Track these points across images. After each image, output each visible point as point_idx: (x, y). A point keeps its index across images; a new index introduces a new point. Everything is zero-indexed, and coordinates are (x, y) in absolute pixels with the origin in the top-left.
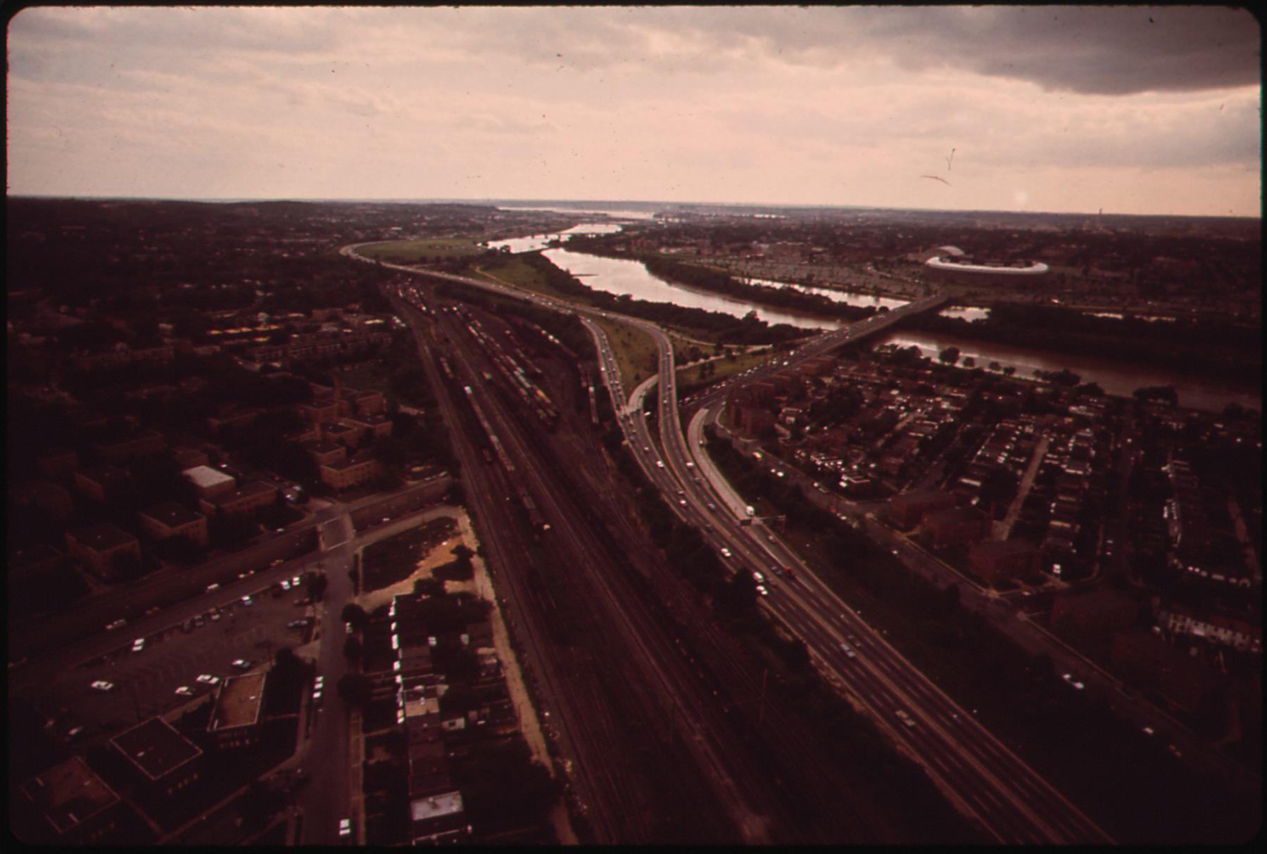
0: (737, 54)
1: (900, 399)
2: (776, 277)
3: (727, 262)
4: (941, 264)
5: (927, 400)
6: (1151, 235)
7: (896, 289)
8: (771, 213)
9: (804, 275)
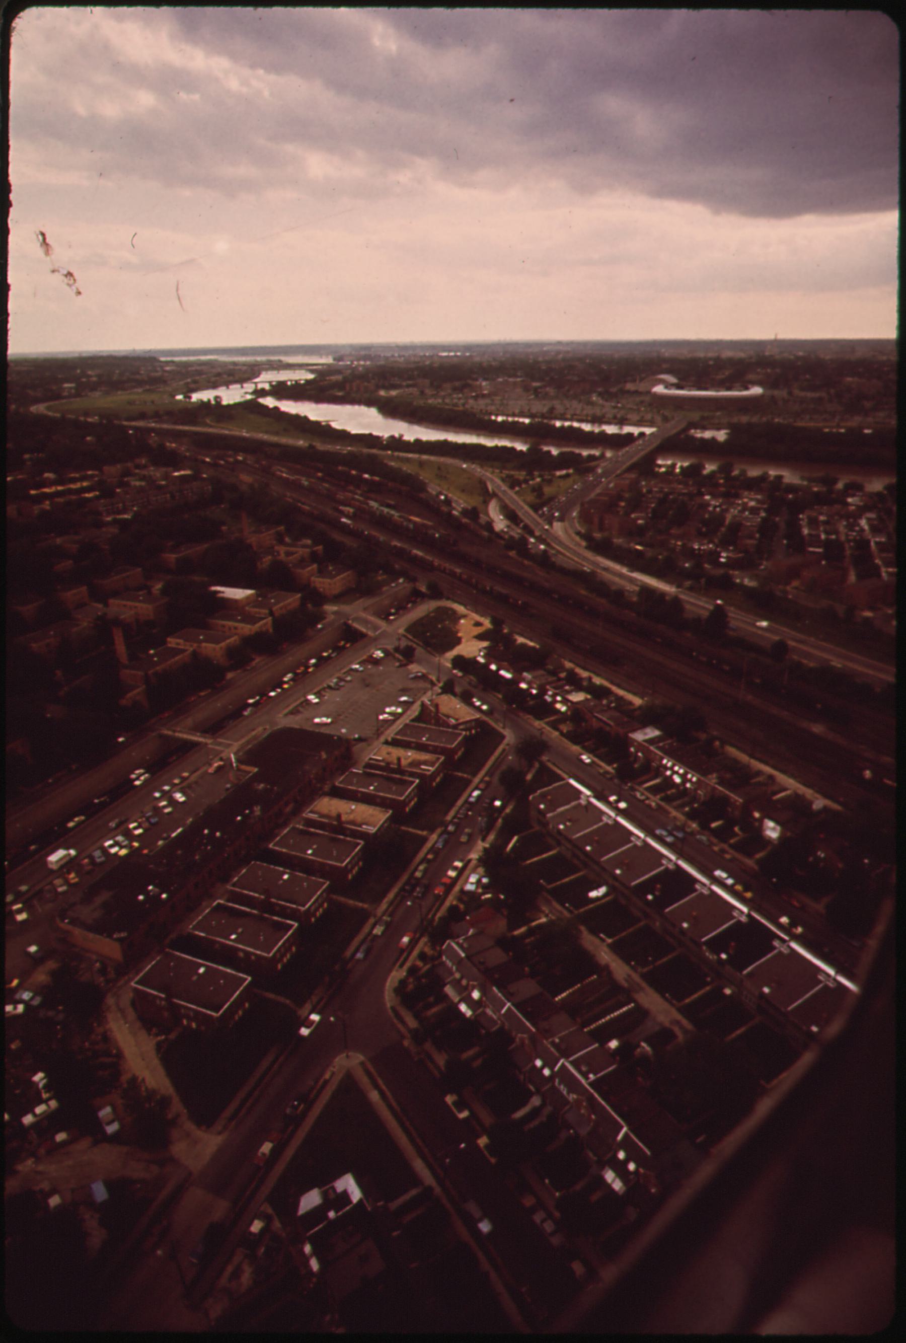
0: (404, 177)
1: (713, 503)
2: (517, 411)
3: (456, 401)
4: (666, 391)
5: (737, 502)
6: (828, 357)
7: (634, 417)
8: (456, 352)
9: (545, 410)
